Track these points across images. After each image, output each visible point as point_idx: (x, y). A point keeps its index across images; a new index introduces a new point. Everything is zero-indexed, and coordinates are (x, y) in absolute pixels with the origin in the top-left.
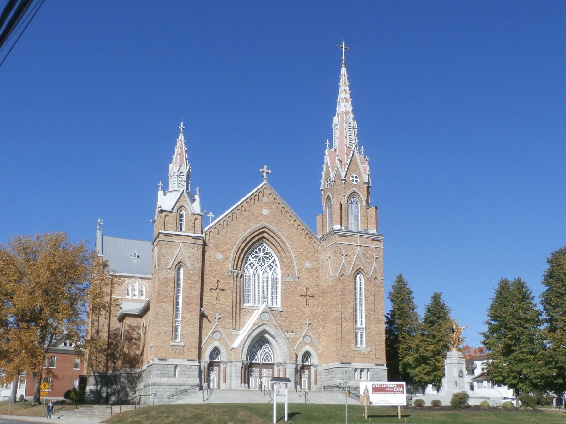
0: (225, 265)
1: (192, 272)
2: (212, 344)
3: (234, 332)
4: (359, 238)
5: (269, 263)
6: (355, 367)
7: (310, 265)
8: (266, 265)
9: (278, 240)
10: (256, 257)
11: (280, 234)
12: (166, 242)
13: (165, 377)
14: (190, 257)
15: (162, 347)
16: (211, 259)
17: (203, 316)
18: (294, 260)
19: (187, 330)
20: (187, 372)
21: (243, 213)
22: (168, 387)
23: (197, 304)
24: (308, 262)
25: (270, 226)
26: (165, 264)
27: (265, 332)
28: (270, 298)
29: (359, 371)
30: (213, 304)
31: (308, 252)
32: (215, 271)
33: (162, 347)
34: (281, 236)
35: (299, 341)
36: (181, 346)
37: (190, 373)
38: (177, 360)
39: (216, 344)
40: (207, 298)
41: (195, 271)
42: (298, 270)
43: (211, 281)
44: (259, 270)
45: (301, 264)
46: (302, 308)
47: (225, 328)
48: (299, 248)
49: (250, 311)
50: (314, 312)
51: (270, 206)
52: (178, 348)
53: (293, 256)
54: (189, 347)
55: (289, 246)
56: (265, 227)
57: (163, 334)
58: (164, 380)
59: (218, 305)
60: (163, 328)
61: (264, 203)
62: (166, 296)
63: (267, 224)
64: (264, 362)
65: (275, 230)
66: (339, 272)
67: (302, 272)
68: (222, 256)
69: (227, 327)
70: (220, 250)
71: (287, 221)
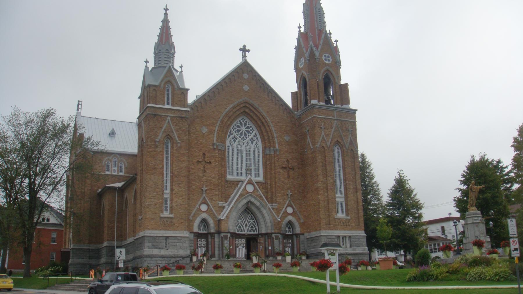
0: (209, 138)
1: (179, 145)
3: (221, 204)
5: (250, 137)
8: (248, 139)
9: (258, 114)
10: (238, 131)
11: (260, 109)
13: (157, 248)
15: (152, 219)
16: (197, 133)
20: (178, 244)
22: (160, 259)
23: (185, 176)
25: (251, 101)
29: (347, 239)
33: (152, 219)
37: (181, 244)
47: (212, 200)
53: (273, 129)
54: (178, 219)
55: (269, 120)
56: (246, 102)
58: (156, 252)
60: (153, 200)
62: (155, 169)
65: (256, 105)
66: (319, 144)
69: (214, 199)
71: (266, 97)
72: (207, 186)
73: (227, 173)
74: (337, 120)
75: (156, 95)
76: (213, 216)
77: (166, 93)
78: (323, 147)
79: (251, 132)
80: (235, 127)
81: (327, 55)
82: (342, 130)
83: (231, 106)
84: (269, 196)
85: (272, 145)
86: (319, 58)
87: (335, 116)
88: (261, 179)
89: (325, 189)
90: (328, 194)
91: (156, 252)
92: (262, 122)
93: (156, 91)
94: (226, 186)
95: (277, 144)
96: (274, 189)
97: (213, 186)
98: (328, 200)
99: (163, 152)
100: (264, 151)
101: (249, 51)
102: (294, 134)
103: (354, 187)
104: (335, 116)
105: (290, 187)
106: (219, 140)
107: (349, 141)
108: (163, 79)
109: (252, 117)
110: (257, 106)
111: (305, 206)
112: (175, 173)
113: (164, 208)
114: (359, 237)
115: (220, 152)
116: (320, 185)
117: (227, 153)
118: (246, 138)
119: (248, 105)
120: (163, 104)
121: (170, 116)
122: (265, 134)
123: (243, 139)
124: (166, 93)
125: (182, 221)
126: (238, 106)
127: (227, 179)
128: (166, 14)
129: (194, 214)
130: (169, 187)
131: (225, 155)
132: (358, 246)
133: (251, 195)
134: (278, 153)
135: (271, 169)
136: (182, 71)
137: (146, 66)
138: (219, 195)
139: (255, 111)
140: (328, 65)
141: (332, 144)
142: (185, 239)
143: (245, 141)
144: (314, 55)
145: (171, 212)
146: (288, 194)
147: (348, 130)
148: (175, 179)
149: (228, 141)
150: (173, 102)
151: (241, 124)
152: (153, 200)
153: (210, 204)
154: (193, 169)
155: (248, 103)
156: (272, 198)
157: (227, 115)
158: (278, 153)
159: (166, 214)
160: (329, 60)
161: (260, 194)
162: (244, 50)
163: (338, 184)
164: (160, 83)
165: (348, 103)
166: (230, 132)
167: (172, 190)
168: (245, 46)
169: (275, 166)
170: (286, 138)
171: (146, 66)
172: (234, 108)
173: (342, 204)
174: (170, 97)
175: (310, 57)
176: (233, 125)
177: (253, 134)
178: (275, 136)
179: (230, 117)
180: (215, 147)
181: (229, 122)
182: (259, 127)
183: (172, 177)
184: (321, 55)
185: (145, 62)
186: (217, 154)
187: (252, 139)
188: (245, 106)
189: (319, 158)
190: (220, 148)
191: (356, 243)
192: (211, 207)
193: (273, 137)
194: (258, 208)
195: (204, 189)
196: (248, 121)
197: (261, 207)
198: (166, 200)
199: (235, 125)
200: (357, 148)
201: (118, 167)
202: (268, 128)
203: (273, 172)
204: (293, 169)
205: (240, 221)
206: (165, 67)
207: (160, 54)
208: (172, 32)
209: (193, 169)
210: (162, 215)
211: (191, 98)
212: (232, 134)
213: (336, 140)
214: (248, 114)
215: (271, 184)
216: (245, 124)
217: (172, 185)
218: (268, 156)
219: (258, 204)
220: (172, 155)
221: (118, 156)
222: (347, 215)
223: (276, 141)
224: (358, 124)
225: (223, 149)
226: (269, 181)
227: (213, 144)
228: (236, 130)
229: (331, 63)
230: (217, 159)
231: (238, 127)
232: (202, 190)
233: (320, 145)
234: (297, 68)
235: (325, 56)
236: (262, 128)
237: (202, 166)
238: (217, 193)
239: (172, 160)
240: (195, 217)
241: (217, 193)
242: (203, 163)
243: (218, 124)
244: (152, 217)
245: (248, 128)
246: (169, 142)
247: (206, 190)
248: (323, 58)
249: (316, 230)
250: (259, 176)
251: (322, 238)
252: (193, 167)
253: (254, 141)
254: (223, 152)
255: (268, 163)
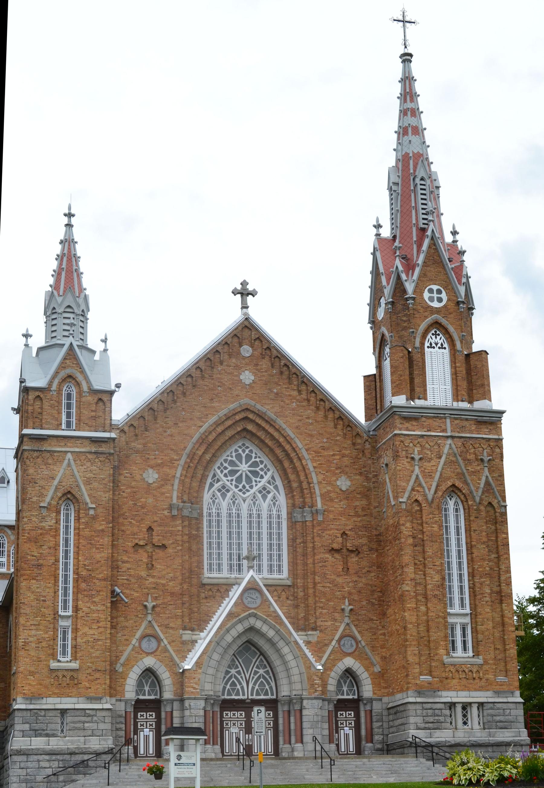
0: (163, 494)
1: (92, 512)
2: (140, 663)
3: (187, 635)
4: (448, 421)
5: (260, 485)
6: (449, 700)
7: (349, 483)
8: (255, 489)
9: (276, 434)
10: (233, 473)
11: (280, 422)
12: (36, 454)
13: (40, 735)
14: (88, 482)
15: (32, 673)
16: (133, 484)
17: (115, 602)
18: (313, 475)
19: (85, 634)
20: (86, 725)
21: (200, 382)
22: (47, 757)
23: (105, 580)
24: (343, 478)
25: (259, 406)
26: (35, 499)
27: (251, 629)
28: (265, 557)
29: (459, 708)
30: (140, 578)
31: (343, 456)
32: (143, 508)
33: (32, 673)
34: (284, 426)
35: (330, 648)
36: (72, 670)
37: (94, 726)
38: (65, 700)
39: (149, 662)
40: (128, 565)
41: (100, 510)
42: (322, 495)
43: (135, 529)
44: (239, 501)
45: (329, 483)
46: (333, 577)
47: (167, 627)
48: (323, 448)
49: (221, 589)
50: (360, 585)
51: (257, 365)
52: (65, 673)
53: (310, 466)
54: (89, 671)
55: (300, 446)
56: (247, 409)
57: (33, 645)
58: (38, 743)
59: (151, 580)
60: (33, 632)
61: (244, 358)
62: (39, 566)
63: (253, 403)
64: (255, 697)
65: (271, 414)
66: (406, 495)
67: (332, 500)
68: (156, 476)
69: (171, 625)
70: (152, 462)
71: (295, 393)
72: (156, 598)
73: (206, 567)
74: (452, 437)
75: (42, 408)
76: (172, 665)
77: (64, 401)
78: (416, 501)
79: (262, 473)
80: (226, 465)
81: (435, 287)
82: (464, 460)
83: (213, 419)
84: (302, 615)
85: (308, 500)
86: (414, 299)
87: (449, 429)
88: (284, 575)
89: (420, 598)
90: (428, 609)
91: (38, 743)
92: (284, 450)
93: (41, 399)
94: (203, 595)
95: (319, 499)
96: (311, 600)
97: (169, 598)
98: (428, 621)
99: (57, 530)
100: (290, 515)
101: (253, 294)
102: (361, 474)
103: (496, 589)
104: (449, 429)
105: (350, 593)
106: (185, 498)
107: (482, 485)
108: (57, 373)
109: (262, 441)
110: (273, 416)
111: (384, 634)
112: (84, 573)
113: (59, 649)
114: (505, 706)
115: (186, 523)
116: (407, 588)
117: (205, 523)
118: (251, 487)
119: (251, 416)
120: (58, 427)
121: (71, 452)
122: (292, 477)
123: (243, 490)
124: (64, 401)
125: (97, 675)
126: (228, 418)
127: (205, 581)
128: (69, 226)
129: (128, 660)
130: (70, 604)
131: (199, 528)
132: (505, 726)
133: (255, 616)
134: (320, 518)
135: (305, 555)
136: (105, 350)
137: (26, 345)
138: (183, 616)
139: (267, 427)
140: (438, 311)
141: (440, 493)
142: (104, 713)
143: (248, 494)
144: (405, 291)
145: (75, 658)
146: (343, 610)
147: (482, 460)
148: (83, 585)
149: (207, 497)
150: (79, 420)
151: (239, 457)
152: (33, 632)
153: (162, 636)
154: (123, 562)
155: (253, 412)
156: (306, 619)
157: (202, 440)
158: (320, 518)
159: (65, 662)
160: (440, 300)
161: (275, 612)
162: (244, 292)
163: (456, 584)
164: (50, 383)
165: (486, 395)
166: (214, 475)
167: (76, 609)
168: (244, 284)
169: (314, 548)
170: (344, 483)
171: (26, 345)
172: (217, 424)
173: (464, 630)
174: (74, 410)
175: (394, 295)
176: (222, 460)
177: (267, 478)
178: (315, 480)
179: (210, 445)
180: (175, 512)
181: (208, 457)
182: (278, 462)
183: (76, 581)
184: (419, 290)
185: (24, 335)
186: (180, 528)
187: (264, 489)
188: (246, 418)
189: (407, 529)
190: (186, 513)
191: (498, 718)
192: (166, 642)
193: (309, 483)
194: (270, 641)
195: (150, 605)
196: (255, 450)
197: (276, 639)
198: (64, 632)
199: (226, 461)
200: (504, 499)
201: (9, 556)
202: (298, 464)
203: (310, 561)
204: (356, 551)
205: (233, 671)
206: (64, 345)
207: (54, 316)
208: (83, 266)
209: (123, 562)
210: (54, 665)
211: (121, 409)
212: (218, 481)
213: (450, 484)
214: (253, 434)
215: (305, 588)
216: (249, 457)
217: (75, 600)
218: (298, 526)
219: (271, 633)
220: (78, 535)
221: (9, 532)
222: (476, 654)
223: (318, 492)
224: (506, 444)
225: (195, 515)
226: (300, 582)
227: (171, 507)
228: (226, 471)
229: (445, 306)
230: (179, 538)
231: (232, 463)
232: (145, 606)
233: (409, 498)
234: (373, 322)
235: (431, 291)
236: (286, 464)
237: (146, 555)
238: (179, 612)
239: (77, 547)
240: (128, 664)
241: (179, 612)
242: (149, 548)
243: (182, 462)
244: (32, 669)
245: (255, 464)
246: (72, 507)
247: (154, 607)
248: (426, 295)
249: (402, 691)
250: (280, 571)
251: (410, 707)
252: (125, 558)
253: (269, 492)
254: (193, 523)
255: (298, 541)
